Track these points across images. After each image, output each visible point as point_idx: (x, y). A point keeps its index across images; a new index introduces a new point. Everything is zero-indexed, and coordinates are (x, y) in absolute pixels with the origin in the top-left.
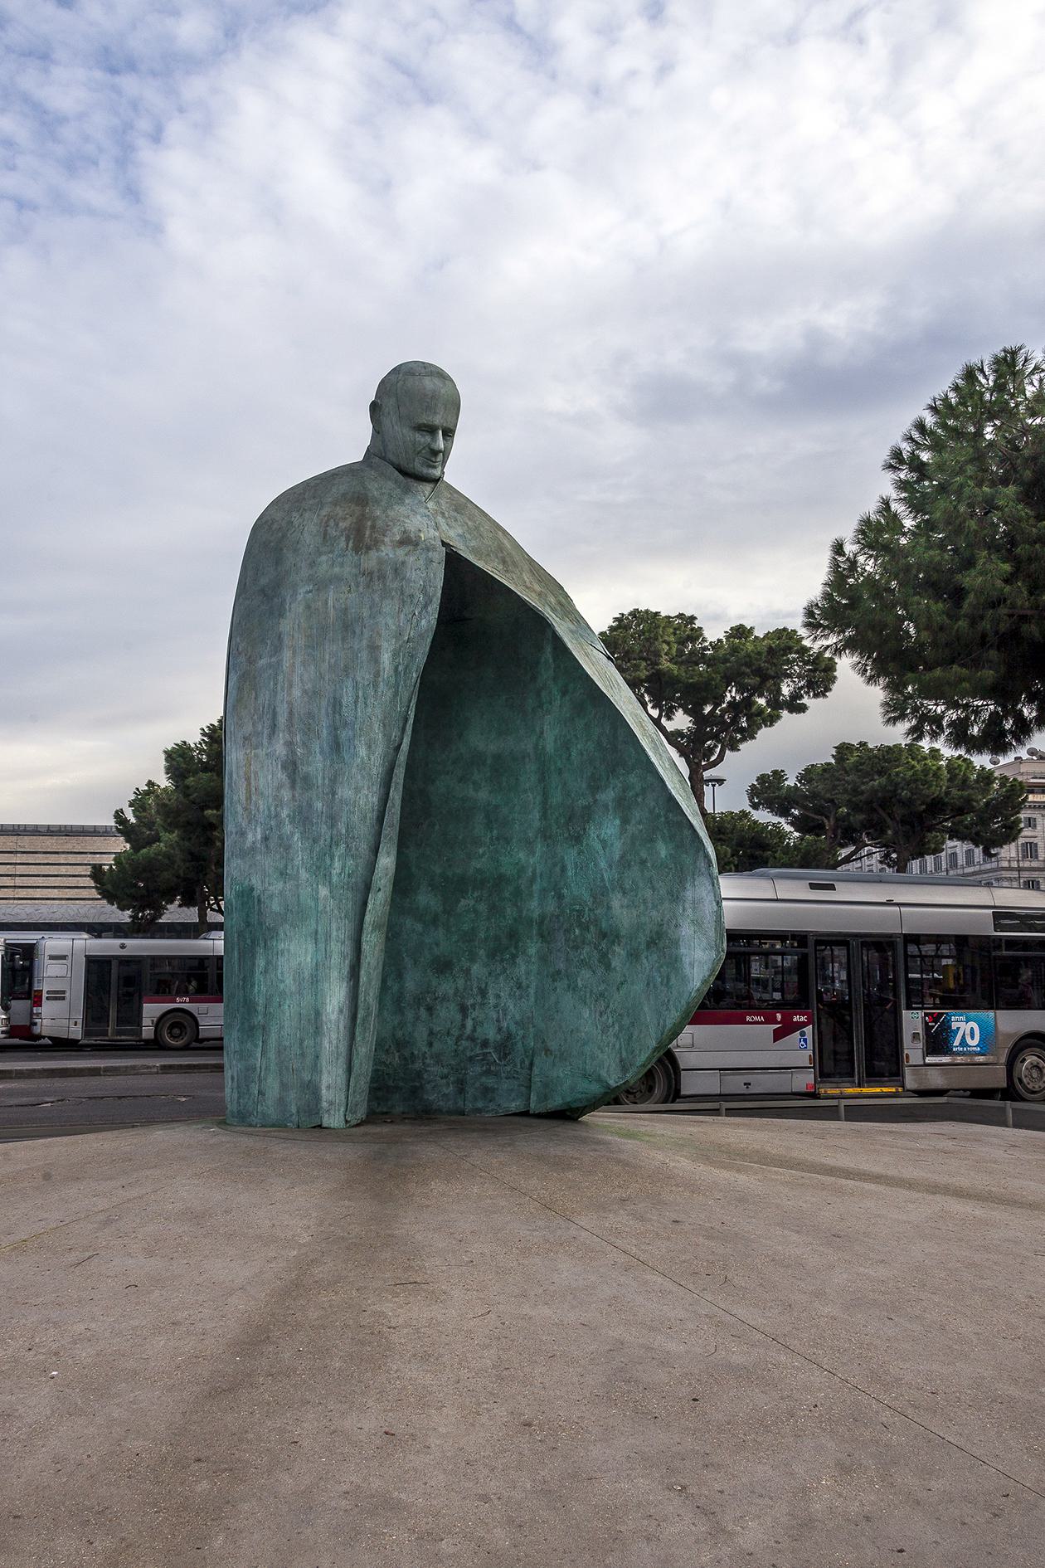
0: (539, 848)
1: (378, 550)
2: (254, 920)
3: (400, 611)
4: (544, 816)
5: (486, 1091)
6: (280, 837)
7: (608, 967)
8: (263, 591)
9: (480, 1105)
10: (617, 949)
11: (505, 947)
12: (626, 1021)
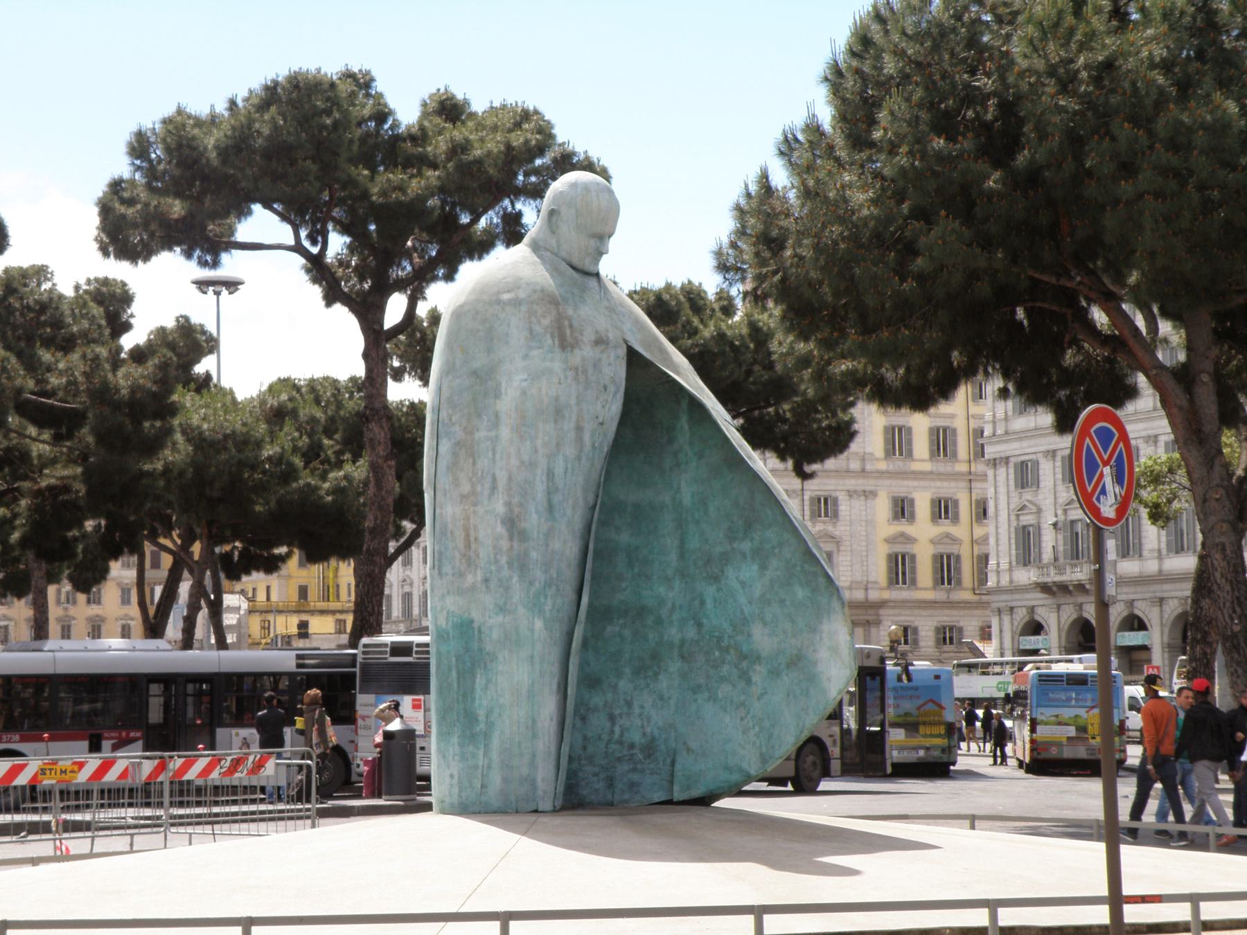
0: (677, 584)
1: (580, 349)
2: (475, 646)
3: (597, 398)
4: (682, 556)
5: (633, 785)
6: (500, 580)
7: (749, 682)
8: (475, 373)
9: (626, 796)
10: (757, 667)
11: (648, 666)
12: (767, 724)
